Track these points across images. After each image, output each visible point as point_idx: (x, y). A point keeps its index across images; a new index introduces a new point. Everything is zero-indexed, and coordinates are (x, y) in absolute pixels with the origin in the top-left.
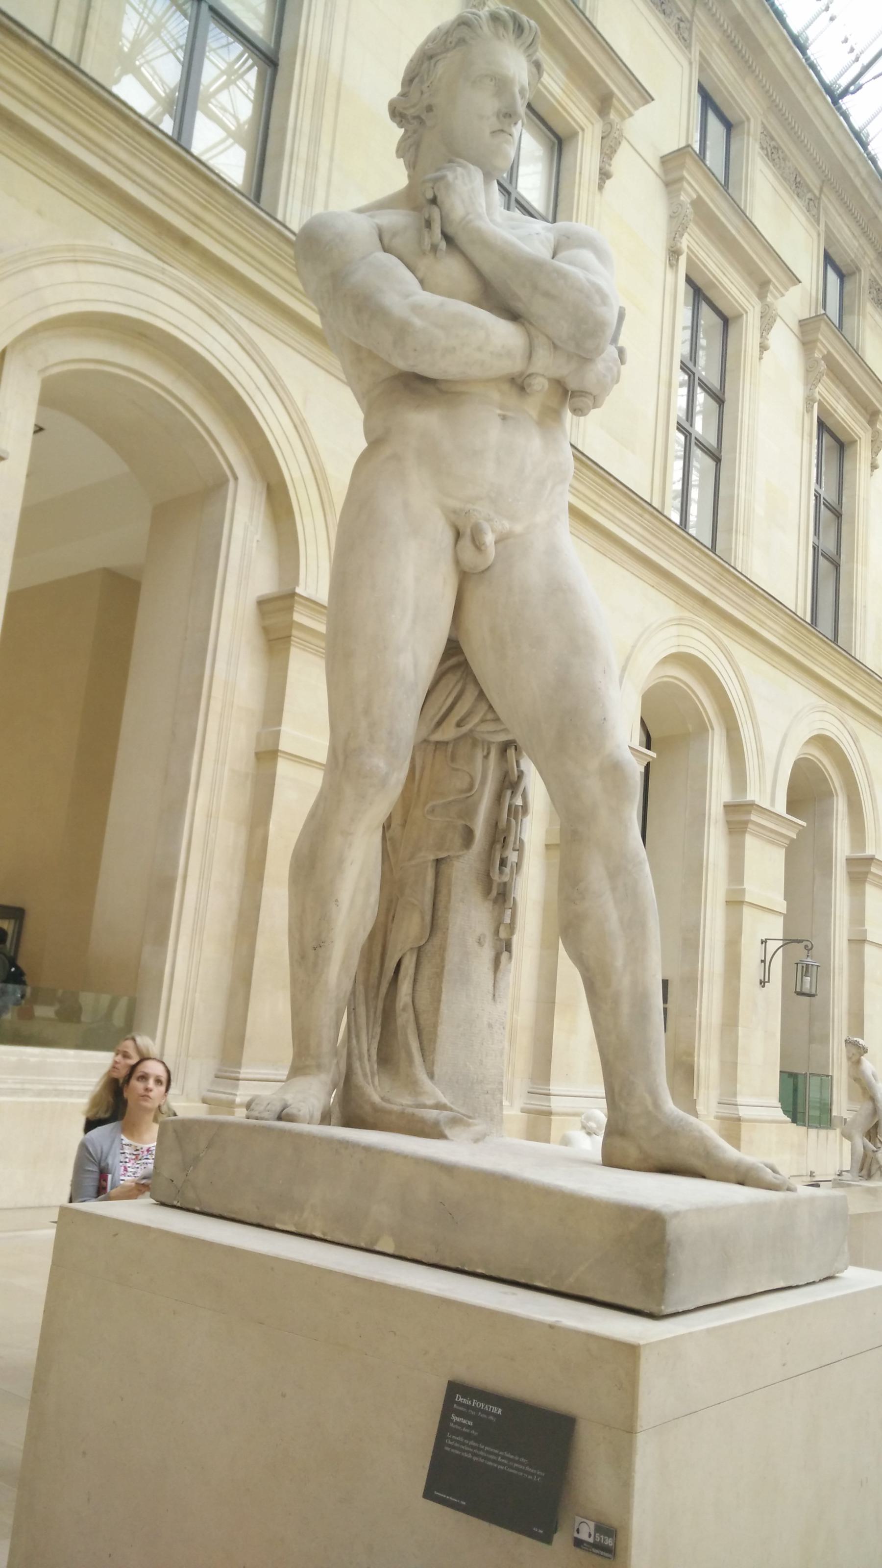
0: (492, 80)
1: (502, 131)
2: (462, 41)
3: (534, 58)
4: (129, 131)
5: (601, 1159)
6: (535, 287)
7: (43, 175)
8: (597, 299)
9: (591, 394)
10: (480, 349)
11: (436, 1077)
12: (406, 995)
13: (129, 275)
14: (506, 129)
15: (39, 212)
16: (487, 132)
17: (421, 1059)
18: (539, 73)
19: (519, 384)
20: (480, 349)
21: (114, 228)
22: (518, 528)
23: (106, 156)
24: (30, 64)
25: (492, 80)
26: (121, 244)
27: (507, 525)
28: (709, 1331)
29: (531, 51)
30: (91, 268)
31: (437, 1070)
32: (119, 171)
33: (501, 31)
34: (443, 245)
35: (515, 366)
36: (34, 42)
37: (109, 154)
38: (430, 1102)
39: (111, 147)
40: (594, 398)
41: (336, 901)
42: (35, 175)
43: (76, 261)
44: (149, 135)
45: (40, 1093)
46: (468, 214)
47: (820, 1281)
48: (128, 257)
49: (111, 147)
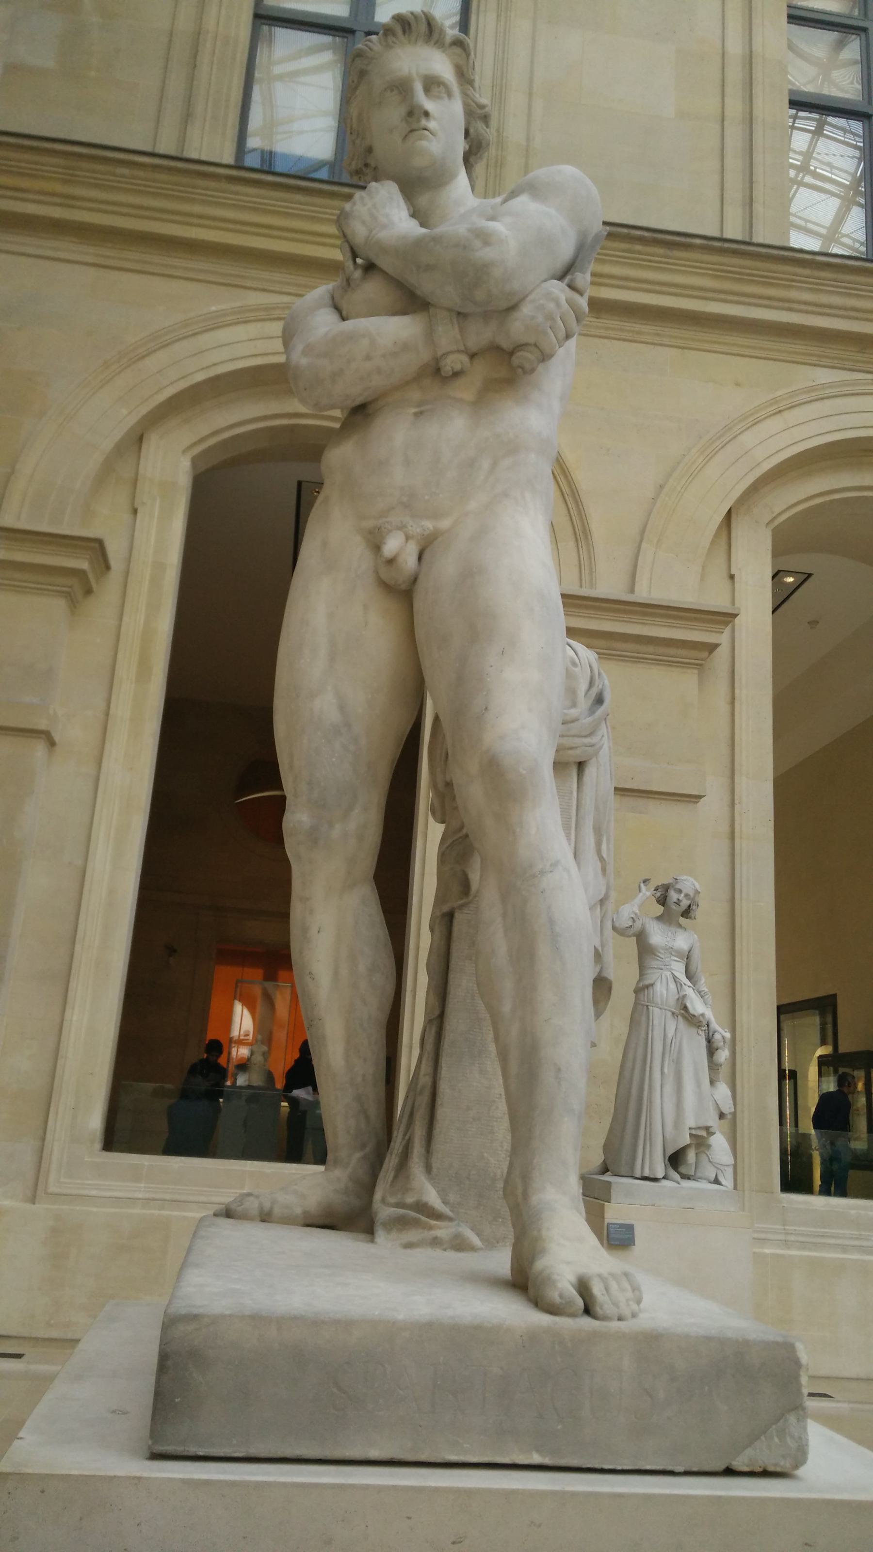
0: (392, 90)
1: (412, 131)
2: (362, 74)
3: (448, 39)
4: (807, 272)
5: (510, 1272)
7: (735, 350)
8: (478, 244)
9: (527, 344)
10: (368, 358)
11: (435, 1170)
12: (425, 1075)
13: (839, 401)
14: (415, 126)
15: (737, 384)
17: (423, 1150)
19: (435, 373)
21: (815, 365)
22: (445, 524)
23: (788, 305)
24: (688, 260)
26: (824, 376)
27: (429, 525)
28: (185, 1482)
29: (436, 36)
30: (796, 411)
31: (435, 1163)
32: (807, 312)
35: (425, 356)
36: (698, 241)
37: (793, 302)
38: (410, 1199)
39: (794, 294)
40: (535, 345)
41: (310, 973)
42: (727, 354)
43: (780, 411)
44: (829, 265)
45: (844, 1249)
46: (371, 231)
47: (687, 1473)
48: (831, 385)
49: (794, 294)
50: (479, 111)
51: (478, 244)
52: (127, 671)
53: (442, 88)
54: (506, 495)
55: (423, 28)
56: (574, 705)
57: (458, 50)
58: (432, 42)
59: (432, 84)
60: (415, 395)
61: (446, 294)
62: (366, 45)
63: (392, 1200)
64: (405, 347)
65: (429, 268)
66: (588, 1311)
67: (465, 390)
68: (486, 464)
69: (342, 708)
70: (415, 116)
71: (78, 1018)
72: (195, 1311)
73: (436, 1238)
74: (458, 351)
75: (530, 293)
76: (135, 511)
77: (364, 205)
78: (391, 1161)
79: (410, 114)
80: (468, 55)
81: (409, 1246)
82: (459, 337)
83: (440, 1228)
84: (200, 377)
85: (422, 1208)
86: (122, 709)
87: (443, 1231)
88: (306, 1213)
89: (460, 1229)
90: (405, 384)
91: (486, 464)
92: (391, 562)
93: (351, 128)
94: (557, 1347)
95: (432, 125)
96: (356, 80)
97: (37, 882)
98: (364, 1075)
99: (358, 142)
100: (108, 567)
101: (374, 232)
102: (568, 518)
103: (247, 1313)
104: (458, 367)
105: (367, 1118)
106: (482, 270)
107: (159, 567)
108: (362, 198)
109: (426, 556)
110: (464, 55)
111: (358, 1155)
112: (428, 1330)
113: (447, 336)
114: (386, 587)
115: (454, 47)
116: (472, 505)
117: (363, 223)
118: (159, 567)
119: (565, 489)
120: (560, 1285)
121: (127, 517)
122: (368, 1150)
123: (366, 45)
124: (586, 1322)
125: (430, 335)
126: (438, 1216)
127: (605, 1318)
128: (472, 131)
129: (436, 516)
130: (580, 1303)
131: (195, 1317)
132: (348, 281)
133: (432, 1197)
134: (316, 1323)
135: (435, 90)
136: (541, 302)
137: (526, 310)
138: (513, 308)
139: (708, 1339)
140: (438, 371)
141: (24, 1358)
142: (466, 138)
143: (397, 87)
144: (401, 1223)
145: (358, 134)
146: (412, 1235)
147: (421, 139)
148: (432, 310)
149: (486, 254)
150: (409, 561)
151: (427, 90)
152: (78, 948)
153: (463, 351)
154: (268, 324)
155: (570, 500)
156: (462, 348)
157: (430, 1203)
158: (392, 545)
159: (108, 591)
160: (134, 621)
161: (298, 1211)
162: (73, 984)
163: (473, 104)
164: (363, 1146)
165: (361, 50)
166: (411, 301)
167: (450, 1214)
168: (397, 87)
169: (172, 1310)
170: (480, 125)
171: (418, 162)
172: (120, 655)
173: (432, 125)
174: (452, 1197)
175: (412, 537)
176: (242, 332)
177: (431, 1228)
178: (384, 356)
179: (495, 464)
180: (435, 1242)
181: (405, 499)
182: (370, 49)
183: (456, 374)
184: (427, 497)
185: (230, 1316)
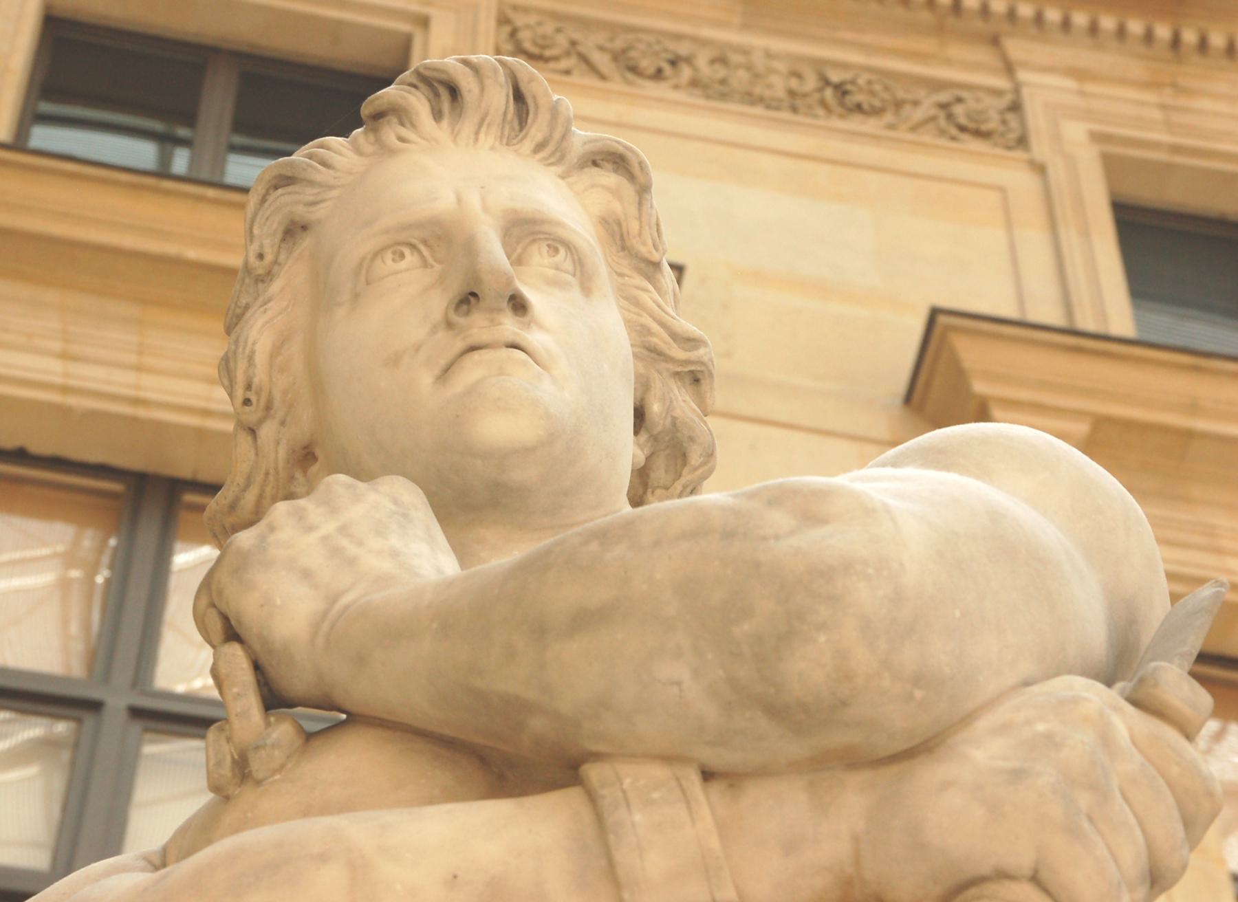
1: (473, 348)
18: (631, 177)
29: (537, 131)
50: (678, 353)
55: (499, 98)
57: (609, 178)
58: (528, 145)
65: (584, 620)
75: (991, 704)
79: (469, 299)
80: (643, 190)
93: (249, 387)
106: (806, 594)
110: (628, 190)
117: (306, 575)
128: (655, 408)
132: (242, 768)
136: (1041, 727)
137: (983, 752)
138: (921, 748)
141: (212, 733)
142: (638, 428)
145: (268, 407)
148: (594, 772)
163: (655, 327)
168: (413, 247)
169: (1117, 312)
170: (683, 402)
171: (497, 428)
182: (325, 164)
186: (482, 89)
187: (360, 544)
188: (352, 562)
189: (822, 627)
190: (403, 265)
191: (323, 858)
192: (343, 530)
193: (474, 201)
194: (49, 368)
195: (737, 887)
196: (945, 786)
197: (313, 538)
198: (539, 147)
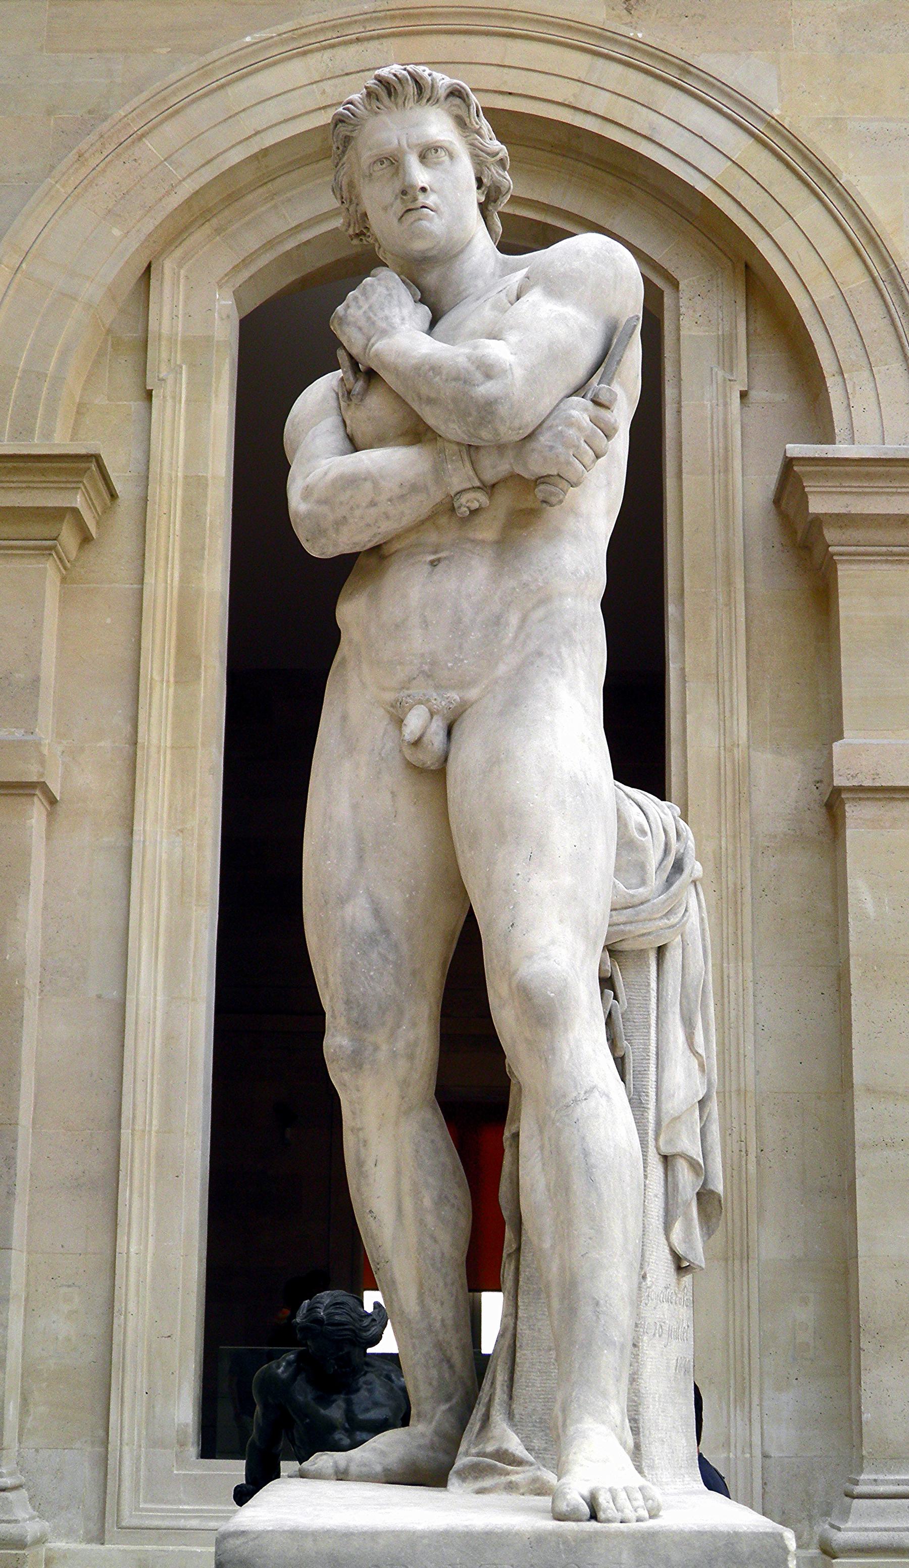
0: (382, 163)
1: (410, 210)
6: (419, 396)
10: (373, 504)
16: (395, 221)
18: (464, 100)
20: (373, 504)
22: (473, 693)
25: (382, 163)
27: (455, 696)
29: (427, 95)
31: (518, 1409)
33: (375, 103)
34: (359, 386)
35: (437, 495)
38: (490, 1448)
40: (558, 475)
41: (371, 1212)
46: (369, 340)
51: (479, 376)
52: (158, 666)
53: (441, 153)
54: (539, 654)
55: (411, 88)
56: (643, 883)
57: (458, 101)
59: (428, 153)
60: (432, 537)
61: (452, 430)
62: (348, 109)
63: (474, 1451)
64: (415, 488)
66: (594, 1516)
67: (487, 531)
68: (514, 619)
69: (377, 913)
70: (409, 199)
71: (138, 1248)
72: (242, 1529)
73: (511, 1482)
74: (474, 488)
76: (149, 395)
77: (360, 307)
78: (478, 1412)
81: (480, 1491)
82: (471, 473)
83: (517, 1473)
84: (236, 157)
85: (504, 1456)
86: (157, 731)
87: (519, 1476)
88: (386, 1470)
89: (539, 1473)
90: (419, 526)
91: (514, 619)
92: (417, 743)
94: (561, 1546)
95: (431, 200)
96: (341, 148)
97: (46, 1033)
98: (443, 1320)
99: (352, 209)
100: (113, 496)
101: (372, 341)
102: (887, 321)
103: (286, 1528)
104: (475, 505)
105: (451, 1366)
106: (487, 410)
107: (196, 484)
108: (356, 298)
109: (456, 734)
110: (463, 106)
111: (444, 1407)
112: (446, 1537)
113: (459, 477)
114: (416, 770)
115: (451, 99)
116: (502, 669)
117: (360, 329)
118: (196, 484)
119: (878, 271)
120: (568, 1497)
121: (135, 405)
122: (454, 1401)
123: (348, 109)
124: (593, 1524)
125: (438, 472)
126: (517, 1462)
127: (608, 1521)
129: (463, 685)
130: (586, 1510)
131: (243, 1533)
133: (514, 1444)
134: (347, 1535)
135: (431, 155)
139: (700, 1534)
140: (453, 509)
142: (479, 188)
143: (386, 158)
144: (476, 1471)
146: (487, 1482)
147: (420, 219)
149: (486, 389)
150: (436, 738)
151: (423, 157)
152: (125, 1133)
153: (479, 488)
154: (340, 52)
155: (888, 290)
156: (478, 484)
157: (510, 1451)
158: (415, 722)
159: (119, 540)
160: (163, 581)
161: (378, 1468)
162: (124, 1195)
164: (448, 1398)
165: (342, 114)
166: (417, 432)
167: (531, 1458)
171: (419, 245)
172: (146, 643)
173: (431, 200)
174: (537, 1443)
175: (438, 712)
176: (297, 71)
177: (508, 1473)
178: (390, 500)
179: (524, 620)
180: (511, 1487)
181: (426, 668)
183: (474, 512)
184: (450, 665)
185: (272, 1531)
186: (403, 88)
187: (375, 315)
188: (373, 323)
189: (489, 422)
190: (384, 166)
191: (365, 479)
192: (370, 307)
193: (404, 143)
194: (220, 541)
195: (480, 479)
196: (533, 450)
197: (361, 312)
198: (428, 101)
